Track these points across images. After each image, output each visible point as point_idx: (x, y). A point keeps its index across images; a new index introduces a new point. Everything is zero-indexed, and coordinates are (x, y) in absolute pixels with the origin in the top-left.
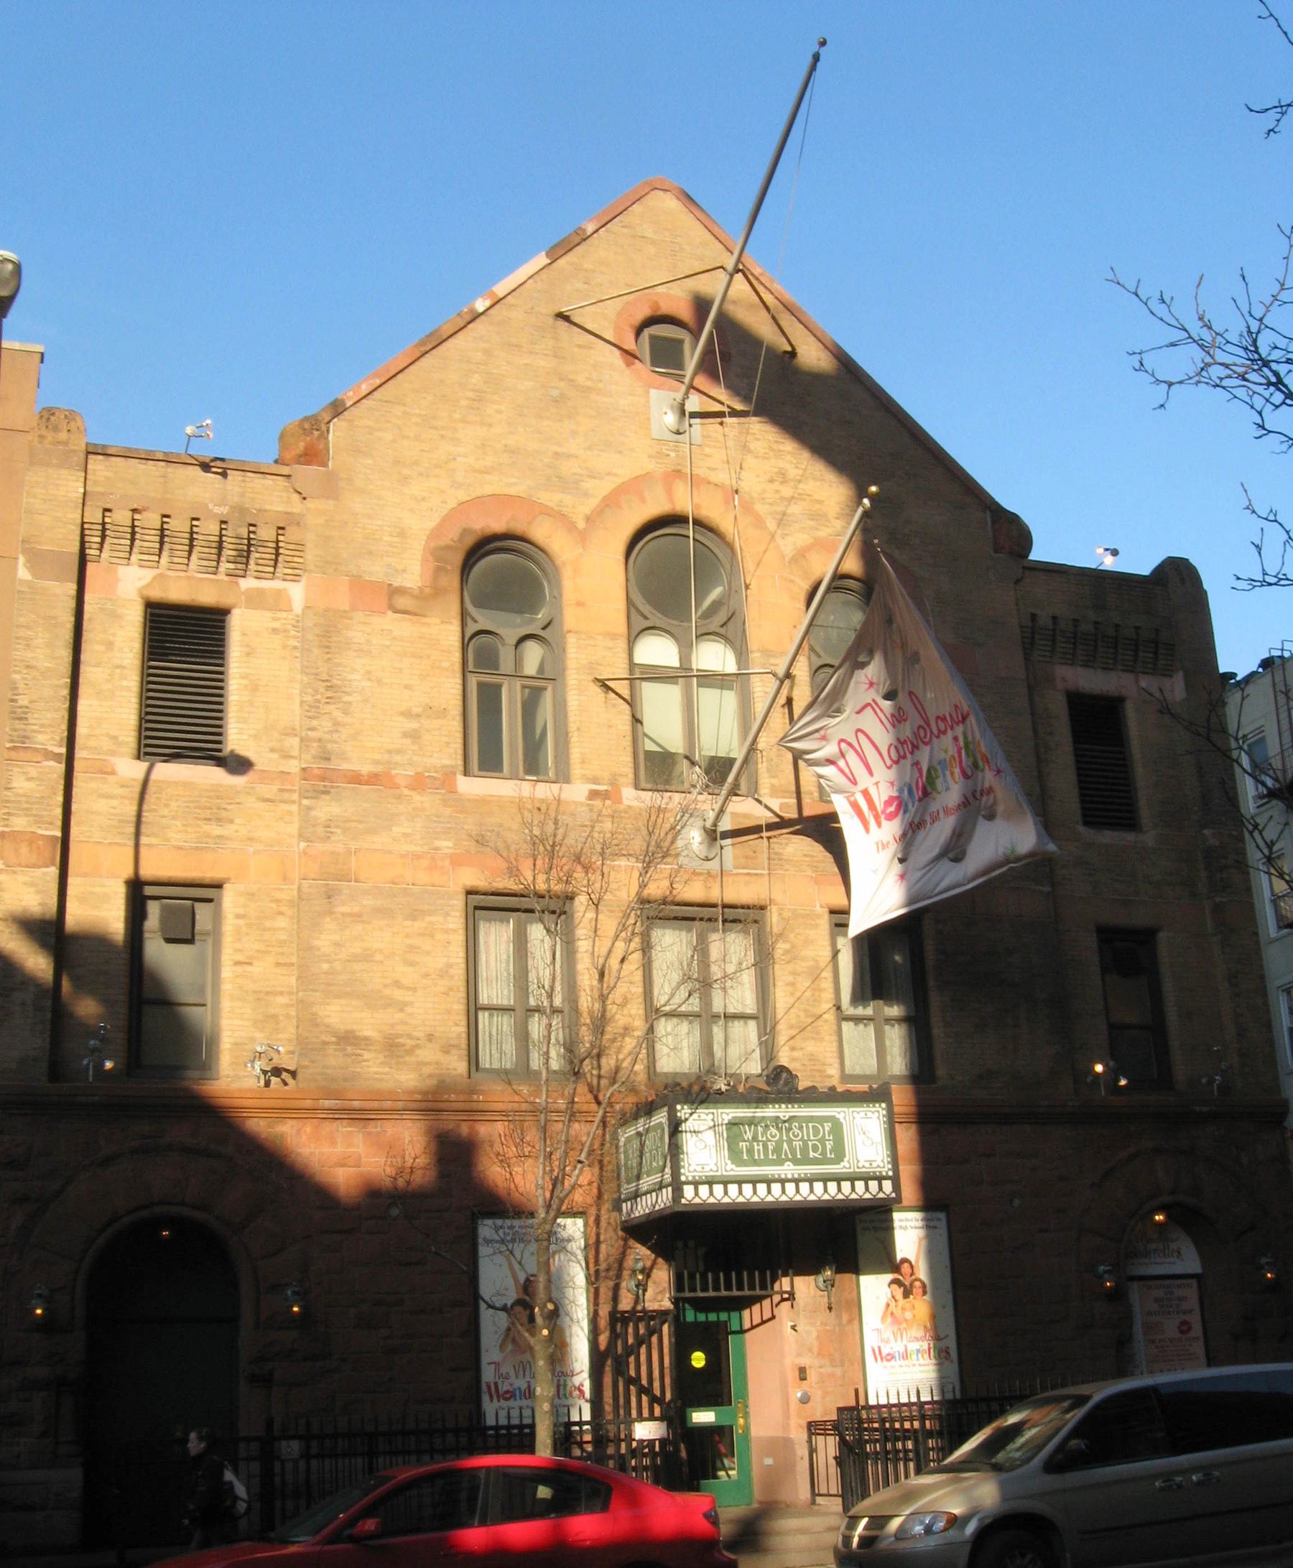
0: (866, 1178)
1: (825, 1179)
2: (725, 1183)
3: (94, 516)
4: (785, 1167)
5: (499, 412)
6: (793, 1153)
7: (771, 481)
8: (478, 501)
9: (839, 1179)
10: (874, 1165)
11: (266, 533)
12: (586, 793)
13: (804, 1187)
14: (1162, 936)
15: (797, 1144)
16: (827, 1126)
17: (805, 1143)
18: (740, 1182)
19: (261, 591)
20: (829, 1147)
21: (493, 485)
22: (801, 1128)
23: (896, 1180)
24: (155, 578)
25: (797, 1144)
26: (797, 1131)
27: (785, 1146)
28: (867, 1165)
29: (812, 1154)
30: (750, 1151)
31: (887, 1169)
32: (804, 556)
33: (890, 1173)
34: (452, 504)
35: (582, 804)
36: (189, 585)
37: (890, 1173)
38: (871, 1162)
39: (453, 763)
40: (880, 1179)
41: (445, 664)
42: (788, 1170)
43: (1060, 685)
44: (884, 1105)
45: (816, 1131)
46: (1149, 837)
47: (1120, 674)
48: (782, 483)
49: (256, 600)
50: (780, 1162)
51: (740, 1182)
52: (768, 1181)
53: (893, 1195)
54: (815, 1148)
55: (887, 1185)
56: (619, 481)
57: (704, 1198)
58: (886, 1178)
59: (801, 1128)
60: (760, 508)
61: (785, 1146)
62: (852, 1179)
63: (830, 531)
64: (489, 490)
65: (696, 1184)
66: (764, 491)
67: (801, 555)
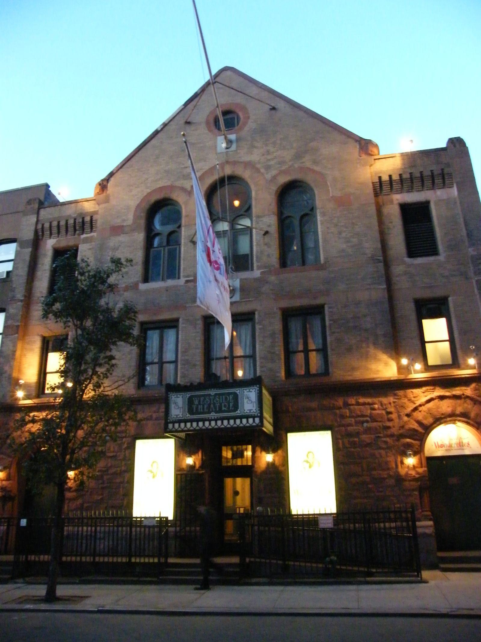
0: (247, 417)
1: (228, 419)
2: (216, 420)
3: (40, 226)
4: (211, 414)
5: (163, 160)
6: (215, 408)
7: (263, 155)
8: (154, 191)
9: (235, 418)
10: (252, 411)
11: (88, 219)
12: (184, 282)
13: (219, 422)
14: (450, 299)
15: (218, 405)
16: (231, 397)
17: (221, 404)
18: (191, 421)
19: (87, 238)
20: (231, 405)
21: (160, 184)
22: (219, 398)
23: (261, 418)
24: (57, 241)
25: (218, 405)
26: (218, 399)
27: (212, 406)
28: (248, 411)
29: (223, 408)
30: (197, 408)
31: (258, 413)
32: (275, 179)
33: (259, 415)
34: (145, 194)
35: (182, 286)
36: (65, 241)
37: (259, 415)
38: (250, 410)
39: (137, 279)
40: (254, 417)
41: (139, 247)
42: (213, 415)
43: (396, 202)
44: (258, 386)
45: (226, 398)
46: (442, 258)
47: (426, 191)
48: (268, 155)
49: (86, 241)
50: (209, 413)
51: (191, 421)
52: (204, 420)
53: (260, 424)
54: (225, 406)
55: (257, 420)
56: (204, 171)
57: (219, 425)
58: (257, 417)
59: (219, 398)
60: (258, 166)
61: (212, 406)
62: (241, 417)
63: (287, 166)
64: (158, 186)
65: (174, 423)
66: (260, 159)
67: (274, 178)
